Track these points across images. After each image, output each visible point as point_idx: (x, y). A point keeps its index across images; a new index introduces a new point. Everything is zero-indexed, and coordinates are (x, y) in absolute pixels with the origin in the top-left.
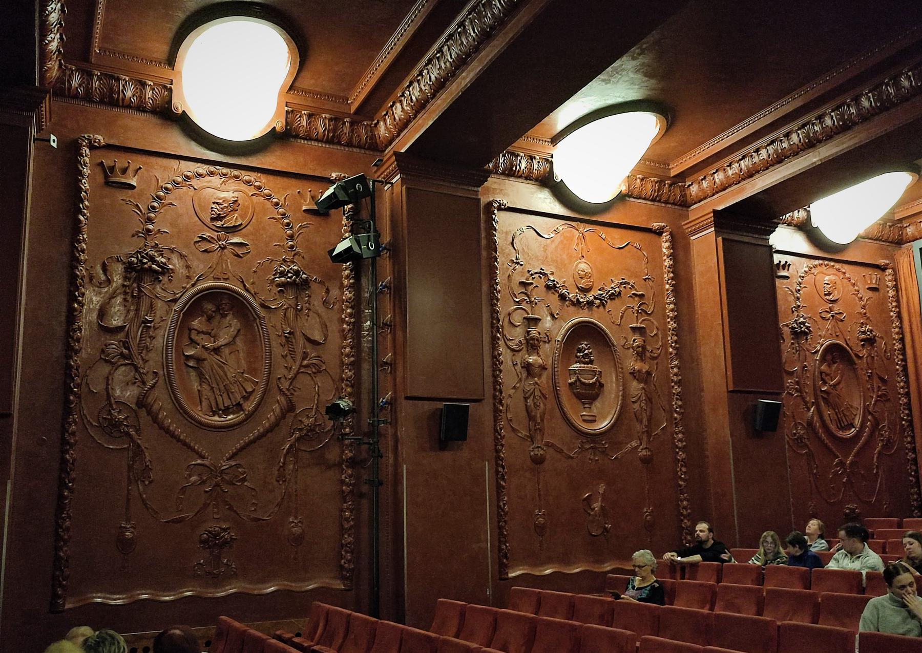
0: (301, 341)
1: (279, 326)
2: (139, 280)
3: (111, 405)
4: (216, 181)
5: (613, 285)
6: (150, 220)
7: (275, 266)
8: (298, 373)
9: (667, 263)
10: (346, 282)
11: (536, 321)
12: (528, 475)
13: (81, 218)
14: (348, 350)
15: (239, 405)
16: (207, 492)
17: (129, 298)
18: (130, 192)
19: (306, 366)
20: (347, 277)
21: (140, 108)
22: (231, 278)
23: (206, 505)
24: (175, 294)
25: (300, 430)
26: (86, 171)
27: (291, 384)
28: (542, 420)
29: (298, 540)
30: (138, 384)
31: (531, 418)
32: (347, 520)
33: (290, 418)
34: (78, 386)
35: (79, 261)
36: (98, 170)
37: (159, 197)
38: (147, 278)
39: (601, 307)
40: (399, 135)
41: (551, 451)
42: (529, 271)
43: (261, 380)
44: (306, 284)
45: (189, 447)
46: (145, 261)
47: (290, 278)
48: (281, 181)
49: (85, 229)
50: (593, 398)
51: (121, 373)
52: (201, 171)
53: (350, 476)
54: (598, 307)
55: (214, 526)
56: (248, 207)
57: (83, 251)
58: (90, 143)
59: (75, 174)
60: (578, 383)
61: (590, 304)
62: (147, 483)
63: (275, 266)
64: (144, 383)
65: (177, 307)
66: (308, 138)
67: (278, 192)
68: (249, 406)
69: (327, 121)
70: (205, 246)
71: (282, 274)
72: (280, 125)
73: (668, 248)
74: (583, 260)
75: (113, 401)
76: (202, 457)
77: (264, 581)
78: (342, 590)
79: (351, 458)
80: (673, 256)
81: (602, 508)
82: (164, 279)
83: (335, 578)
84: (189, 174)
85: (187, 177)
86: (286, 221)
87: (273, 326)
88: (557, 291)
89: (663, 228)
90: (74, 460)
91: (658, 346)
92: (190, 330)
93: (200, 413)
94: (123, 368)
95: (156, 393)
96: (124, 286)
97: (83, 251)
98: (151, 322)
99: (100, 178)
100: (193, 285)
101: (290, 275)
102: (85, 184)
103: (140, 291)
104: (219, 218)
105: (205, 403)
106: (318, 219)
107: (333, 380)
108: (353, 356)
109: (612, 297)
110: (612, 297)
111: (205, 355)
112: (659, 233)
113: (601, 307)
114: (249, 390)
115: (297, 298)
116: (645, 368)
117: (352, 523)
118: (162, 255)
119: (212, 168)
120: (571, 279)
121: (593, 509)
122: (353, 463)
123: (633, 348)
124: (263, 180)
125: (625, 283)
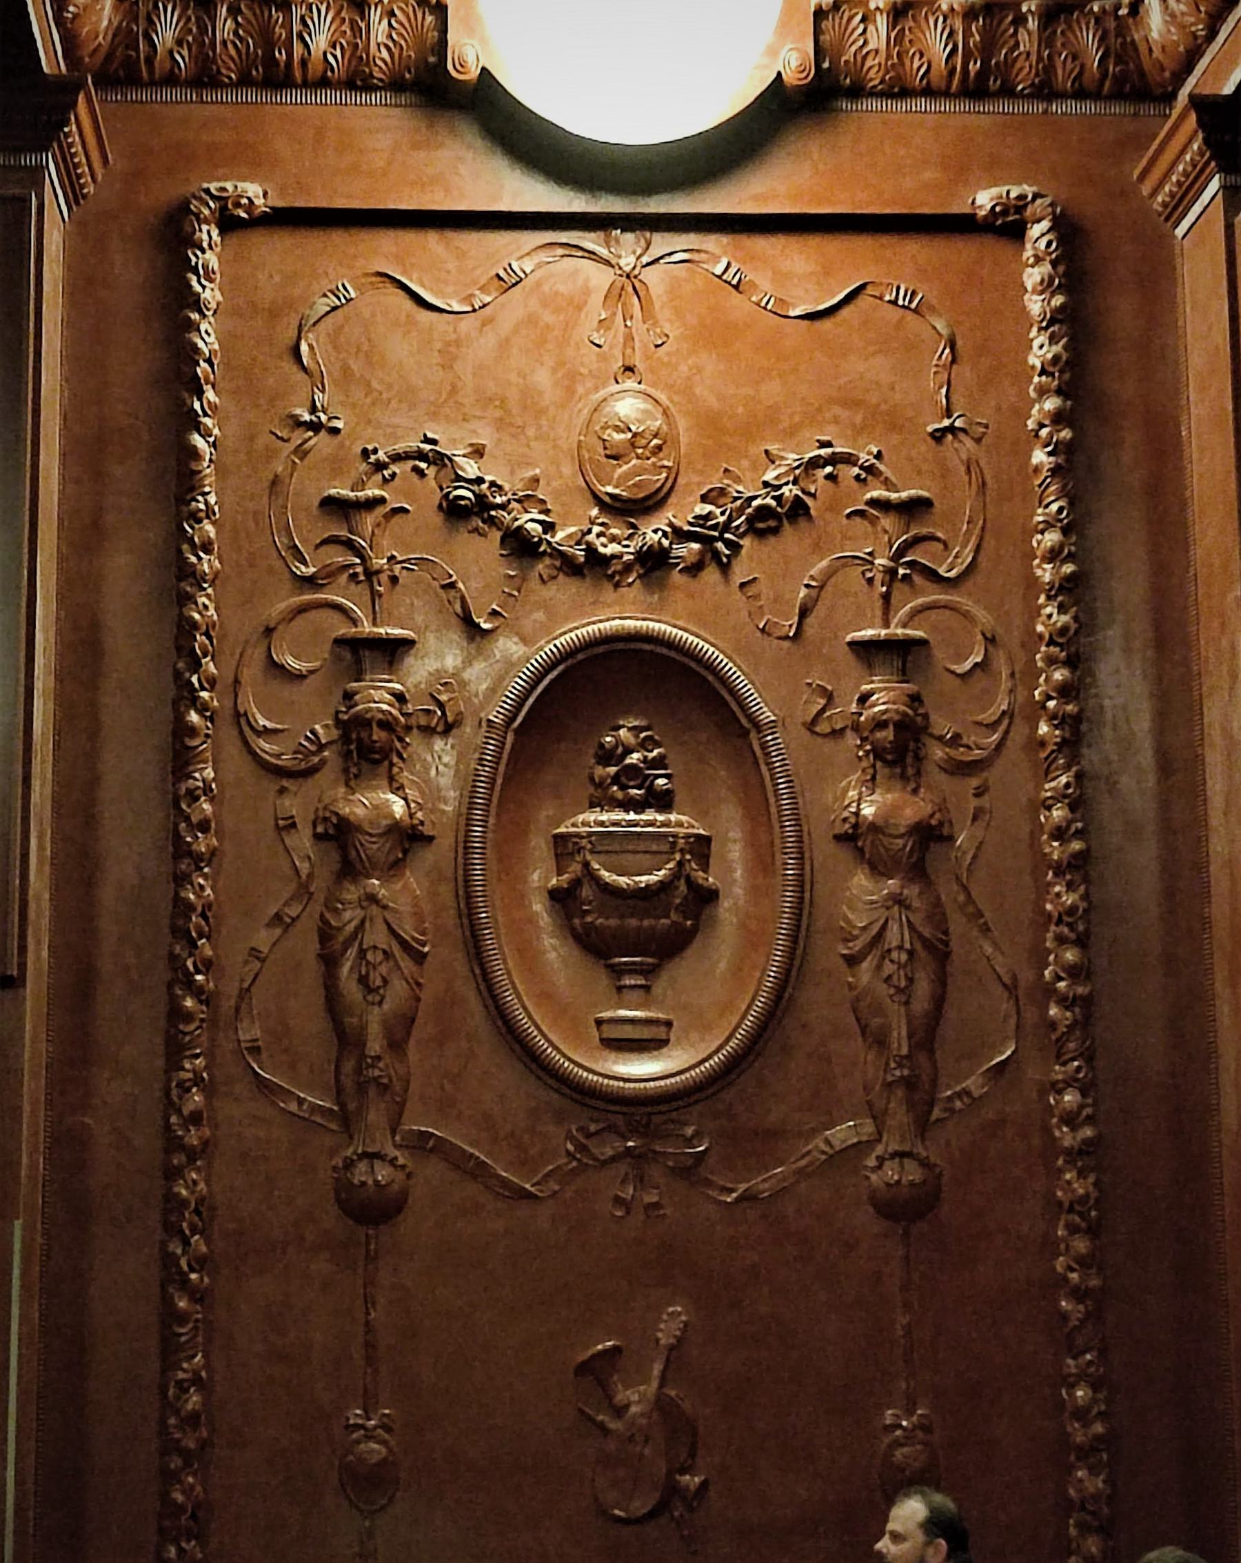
5: (765, 475)
9: (1041, 350)
11: (392, 651)
12: (321, 1265)
13: (198, 441)
14: (1058, 813)
21: (357, 81)
28: (396, 1045)
31: (347, 1039)
32: (1081, 1414)
34: (207, 966)
35: (198, 580)
39: (711, 574)
40: (1212, 34)
41: (433, 1171)
42: (365, 453)
50: (671, 946)
54: (694, 569)
57: (207, 547)
58: (224, 209)
60: (586, 892)
61: (653, 563)
66: (898, 90)
69: (958, 25)
72: (793, 60)
73: (1046, 286)
74: (630, 384)
80: (1072, 321)
81: (662, 1405)
88: (491, 521)
89: (1021, 204)
91: (990, 715)
109: (765, 523)
110: (765, 523)
112: (1008, 226)
113: (711, 574)
116: (914, 809)
117: (1099, 1428)
120: (568, 469)
121: (620, 1411)
123: (856, 727)
125: (834, 460)
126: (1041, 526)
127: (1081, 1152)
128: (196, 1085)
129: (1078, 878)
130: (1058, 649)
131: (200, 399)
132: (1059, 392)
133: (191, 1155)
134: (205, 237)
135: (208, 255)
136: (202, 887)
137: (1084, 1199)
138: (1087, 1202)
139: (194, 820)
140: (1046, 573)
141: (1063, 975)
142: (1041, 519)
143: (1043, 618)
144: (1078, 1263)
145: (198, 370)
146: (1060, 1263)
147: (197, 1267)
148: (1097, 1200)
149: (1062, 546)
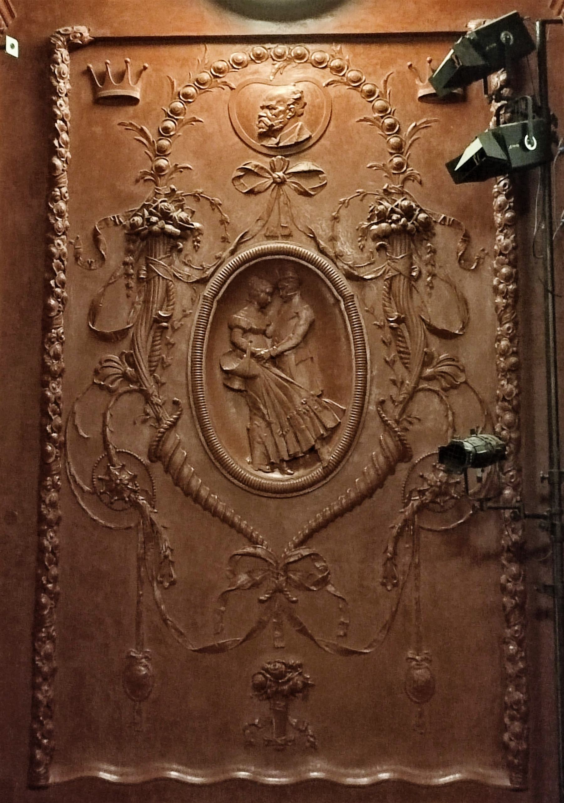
0: (420, 331)
1: (379, 311)
2: (147, 254)
3: (110, 460)
4: (266, 69)
6: (161, 152)
7: (371, 203)
8: (415, 390)
10: (498, 218)
13: (57, 162)
14: (504, 343)
15: (313, 450)
16: (261, 601)
17: (132, 283)
18: (131, 110)
19: (429, 379)
20: (501, 208)
22: (296, 233)
23: (261, 625)
24: (203, 270)
25: (422, 493)
26: (64, 86)
27: (403, 411)
29: (424, 691)
30: (151, 422)
32: (512, 659)
33: (403, 469)
34: (58, 429)
36: (84, 83)
37: (175, 112)
38: (161, 248)
43: (350, 406)
44: (426, 229)
45: (232, 525)
46: (154, 219)
47: (398, 220)
48: (377, 52)
49: (64, 179)
51: (129, 404)
52: (241, 57)
53: (515, 578)
55: (272, 661)
56: (320, 108)
57: (60, 214)
59: (46, 93)
62: (167, 584)
63: (371, 203)
64: (159, 420)
65: (207, 291)
67: (375, 72)
68: (329, 453)
70: (250, 183)
71: (383, 217)
75: (113, 452)
76: (254, 542)
77: (361, 762)
78: (507, 788)
79: (515, 543)
82: (187, 246)
83: (495, 765)
84: (221, 65)
85: (218, 70)
86: (388, 121)
87: (367, 311)
90: (55, 547)
92: (231, 328)
93: (249, 468)
94: (125, 398)
95: (178, 435)
96: (125, 264)
97: (60, 214)
98: (167, 319)
99: (87, 96)
100: (233, 252)
101: (395, 217)
102: (63, 107)
103: (149, 270)
104: (271, 132)
105: (259, 451)
106: (447, 109)
107: (481, 402)
108: (515, 354)
111: (256, 368)
114: (330, 424)
115: (410, 257)
117: (521, 665)
118: (181, 207)
119: (259, 49)
122: (519, 553)
124: (342, 54)
126: (495, 195)
127: (509, 370)
128: (48, 639)
129: (513, 376)
130: (504, 258)
131: (58, 139)
132: (509, 264)
133: (55, 376)
134: (59, 55)
135: (62, 65)
136: (54, 389)
137: (510, 394)
138: (511, 395)
139: (52, 353)
140: (498, 218)
141: (510, 580)
142: (496, 190)
143: (497, 242)
144: (512, 578)
145: (56, 125)
146: (506, 737)
147: (52, 581)
148: (517, 395)
149: (505, 204)
